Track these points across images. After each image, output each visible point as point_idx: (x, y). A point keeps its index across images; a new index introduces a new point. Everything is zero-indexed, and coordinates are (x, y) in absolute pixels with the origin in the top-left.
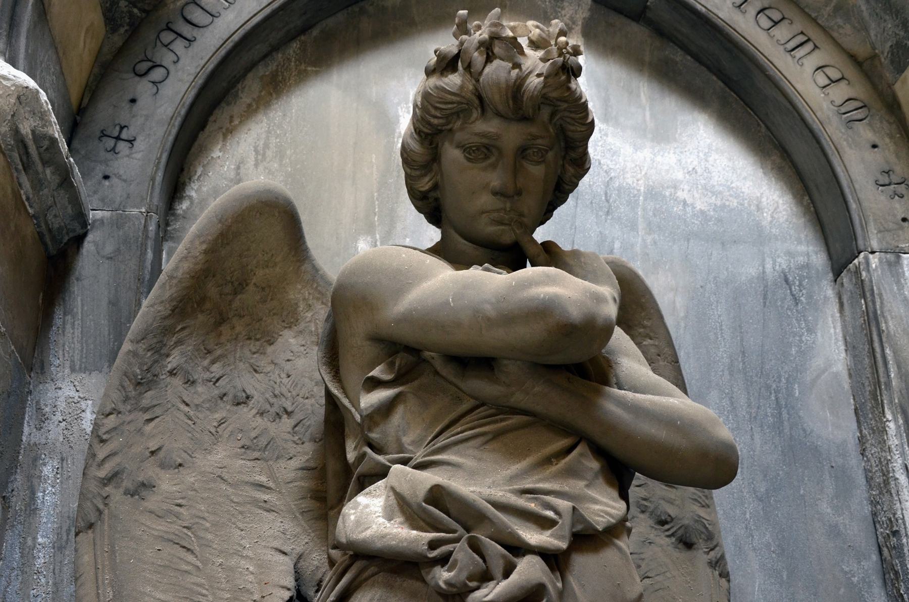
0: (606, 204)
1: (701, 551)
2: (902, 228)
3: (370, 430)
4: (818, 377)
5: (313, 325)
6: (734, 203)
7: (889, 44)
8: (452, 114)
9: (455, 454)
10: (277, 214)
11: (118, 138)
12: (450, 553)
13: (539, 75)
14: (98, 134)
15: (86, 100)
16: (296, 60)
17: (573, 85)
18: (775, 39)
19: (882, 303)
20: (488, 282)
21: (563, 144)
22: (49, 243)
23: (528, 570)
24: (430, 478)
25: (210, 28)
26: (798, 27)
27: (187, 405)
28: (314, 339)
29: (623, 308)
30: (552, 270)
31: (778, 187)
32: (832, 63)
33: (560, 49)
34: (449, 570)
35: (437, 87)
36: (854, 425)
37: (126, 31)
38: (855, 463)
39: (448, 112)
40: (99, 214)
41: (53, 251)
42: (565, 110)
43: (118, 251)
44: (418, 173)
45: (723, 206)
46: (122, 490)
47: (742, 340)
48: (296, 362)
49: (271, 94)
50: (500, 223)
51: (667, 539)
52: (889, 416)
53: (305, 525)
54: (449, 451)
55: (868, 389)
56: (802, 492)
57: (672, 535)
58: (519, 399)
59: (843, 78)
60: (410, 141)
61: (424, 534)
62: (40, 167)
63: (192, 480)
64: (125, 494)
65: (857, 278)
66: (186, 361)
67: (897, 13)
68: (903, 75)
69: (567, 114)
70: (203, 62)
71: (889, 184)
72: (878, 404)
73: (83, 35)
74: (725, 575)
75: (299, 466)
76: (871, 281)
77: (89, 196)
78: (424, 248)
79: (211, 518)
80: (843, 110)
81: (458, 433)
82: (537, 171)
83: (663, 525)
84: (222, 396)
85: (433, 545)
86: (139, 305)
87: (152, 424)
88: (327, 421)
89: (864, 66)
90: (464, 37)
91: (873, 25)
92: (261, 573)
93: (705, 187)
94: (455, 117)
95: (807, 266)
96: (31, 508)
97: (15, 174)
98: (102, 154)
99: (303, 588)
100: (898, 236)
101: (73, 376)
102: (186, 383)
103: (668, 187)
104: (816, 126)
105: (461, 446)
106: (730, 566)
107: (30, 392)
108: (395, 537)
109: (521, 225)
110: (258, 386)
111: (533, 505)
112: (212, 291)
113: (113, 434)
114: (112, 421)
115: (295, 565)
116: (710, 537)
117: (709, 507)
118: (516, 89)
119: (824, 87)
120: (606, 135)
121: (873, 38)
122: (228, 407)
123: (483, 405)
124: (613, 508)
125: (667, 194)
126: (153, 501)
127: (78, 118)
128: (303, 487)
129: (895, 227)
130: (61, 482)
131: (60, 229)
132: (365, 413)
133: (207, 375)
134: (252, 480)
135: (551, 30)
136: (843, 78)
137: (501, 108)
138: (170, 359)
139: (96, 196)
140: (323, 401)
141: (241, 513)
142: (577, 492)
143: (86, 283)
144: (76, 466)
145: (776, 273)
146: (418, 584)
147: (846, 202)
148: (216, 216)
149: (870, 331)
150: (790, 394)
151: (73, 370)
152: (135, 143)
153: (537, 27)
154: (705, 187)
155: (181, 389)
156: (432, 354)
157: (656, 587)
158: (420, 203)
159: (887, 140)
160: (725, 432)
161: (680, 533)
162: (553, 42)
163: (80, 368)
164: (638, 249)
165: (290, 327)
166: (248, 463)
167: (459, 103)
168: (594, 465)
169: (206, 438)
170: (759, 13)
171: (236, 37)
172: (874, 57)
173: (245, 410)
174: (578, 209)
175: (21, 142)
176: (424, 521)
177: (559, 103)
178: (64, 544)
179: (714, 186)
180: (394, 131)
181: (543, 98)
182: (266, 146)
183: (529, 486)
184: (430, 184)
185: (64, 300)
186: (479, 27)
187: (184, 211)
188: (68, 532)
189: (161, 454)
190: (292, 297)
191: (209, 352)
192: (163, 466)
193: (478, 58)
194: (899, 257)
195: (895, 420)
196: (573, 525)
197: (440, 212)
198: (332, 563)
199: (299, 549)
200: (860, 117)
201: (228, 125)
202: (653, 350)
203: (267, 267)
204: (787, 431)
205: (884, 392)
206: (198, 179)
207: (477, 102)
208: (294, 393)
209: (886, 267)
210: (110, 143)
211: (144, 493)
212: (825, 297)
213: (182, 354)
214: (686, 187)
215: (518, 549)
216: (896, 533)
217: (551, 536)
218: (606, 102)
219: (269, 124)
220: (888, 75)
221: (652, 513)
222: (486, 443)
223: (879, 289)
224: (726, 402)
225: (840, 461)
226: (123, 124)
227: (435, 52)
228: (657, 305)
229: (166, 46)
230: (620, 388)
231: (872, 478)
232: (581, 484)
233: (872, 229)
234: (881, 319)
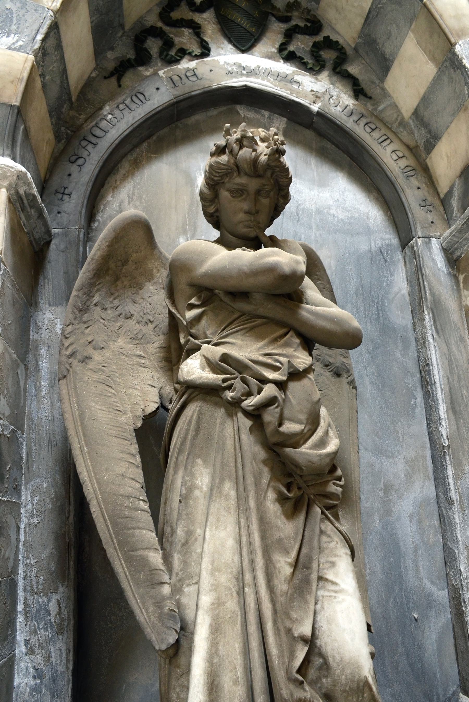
0: (297, 217)
1: (344, 378)
2: (431, 226)
3: (191, 328)
4: (395, 296)
5: (160, 279)
6: (357, 215)
7: (423, 141)
8: (224, 175)
9: (232, 338)
10: (141, 226)
11: (63, 194)
13: (265, 155)
14: (54, 192)
15: (48, 176)
16: (146, 152)
17: (282, 159)
18: (373, 138)
19: (423, 261)
20: (244, 256)
21: (277, 188)
22: (35, 245)
23: (269, 390)
24: (221, 350)
25: (105, 138)
26: (384, 131)
27: (104, 320)
28: (161, 286)
29: (307, 267)
30: (275, 249)
31: (376, 207)
32: (399, 149)
33: (275, 142)
34: (232, 392)
35: (216, 162)
36: (411, 318)
37: (65, 142)
38: (411, 335)
39: (222, 174)
40: (57, 230)
41: (37, 249)
42: (278, 171)
43: (66, 247)
44: (208, 204)
45: (352, 217)
46: (77, 360)
47: (361, 280)
48: (154, 298)
49: (134, 169)
50: (249, 227)
51: (329, 373)
53: (162, 374)
54: (229, 337)
55: (417, 301)
56: (388, 349)
57: (331, 371)
58: (261, 311)
59: (404, 156)
60: (204, 188)
61: (220, 376)
62: (29, 210)
63: (109, 354)
64: (79, 362)
65: (412, 250)
66: (102, 299)
67: (426, 126)
68: (430, 155)
69: (279, 173)
70: (102, 154)
71: (425, 206)
72: (421, 308)
73: (45, 144)
74: (355, 388)
75: (158, 346)
77: (52, 222)
78: (212, 241)
79: (119, 372)
80: (405, 171)
81: (233, 329)
82: (265, 201)
83: (327, 367)
85: (224, 381)
86: (78, 273)
87: (89, 329)
88: (170, 325)
89: (413, 150)
90: (229, 137)
91: (416, 132)
92: (144, 396)
93: (343, 208)
94: (225, 176)
95: (390, 245)
96: (37, 369)
97: (18, 213)
98: (57, 202)
99: (163, 402)
100: (430, 230)
101: (50, 308)
102: (103, 309)
103: (326, 208)
104: (393, 179)
105: (235, 335)
106: (357, 384)
107: (32, 316)
108: (206, 378)
109: (259, 228)
110: (136, 310)
111: (270, 361)
112: (112, 265)
113: (71, 334)
114: (70, 328)
115: (159, 392)
116: (348, 371)
117: (347, 357)
118: (255, 161)
119: (396, 160)
121: (416, 138)
122: (123, 320)
123: (244, 314)
124: (307, 360)
125: (326, 211)
126: (91, 365)
127: (45, 185)
128: (160, 356)
129: (428, 225)
130: (49, 357)
131: (39, 239)
132: (188, 321)
133: (112, 305)
134: (136, 354)
135: (270, 133)
136: (404, 156)
137: (247, 171)
138: (94, 298)
139: (55, 222)
140: (167, 315)
141: (132, 369)
142: (290, 354)
143: (53, 263)
144: (55, 350)
145: (376, 248)
146: (218, 399)
147: (407, 214)
148: (112, 229)
149: (418, 274)
150: (383, 305)
151: (50, 305)
152: (72, 196)
153: (263, 131)
154: (343, 208)
155: (100, 312)
156: (219, 291)
157: (325, 394)
158: (209, 219)
159: (424, 185)
160: (355, 323)
161: (335, 370)
162: (271, 139)
163: (53, 304)
164: (313, 238)
165: (150, 281)
166: (134, 346)
167: (227, 169)
168: (297, 341)
169: (114, 335)
170: (365, 125)
171: (117, 142)
172: (417, 146)
173: (131, 321)
174: (284, 220)
175: (20, 198)
176: (219, 370)
177: (275, 168)
178: (53, 385)
179: (347, 207)
180: (194, 184)
181: (268, 166)
182: (133, 194)
183: (268, 351)
184: (214, 209)
185: (43, 272)
186: (235, 132)
187: (96, 227)
188: (55, 379)
189: (94, 343)
190: (150, 266)
191: (112, 294)
192: (95, 348)
193: (236, 147)
194: (430, 240)
195: (429, 314)
196: (289, 369)
197: (219, 223)
198: (176, 391)
199: (161, 385)
200: (412, 174)
201: (115, 185)
202: (321, 286)
203: (137, 252)
204: (382, 321)
205: (424, 302)
206: (102, 211)
207: (236, 168)
208: (153, 312)
209: (425, 245)
210: (60, 196)
211: (87, 361)
212: (398, 259)
213: (100, 295)
214: (334, 208)
215: (264, 381)
216: (427, 365)
217: (279, 374)
218: (295, 167)
219: (134, 183)
220: (424, 155)
221: (322, 362)
222: (247, 332)
223: (422, 254)
224: (355, 310)
225: (405, 334)
226: (65, 187)
227: (215, 145)
228: (323, 264)
229: (84, 148)
230: (307, 304)
231: (418, 341)
232: (292, 350)
233: (419, 227)
234: (423, 269)
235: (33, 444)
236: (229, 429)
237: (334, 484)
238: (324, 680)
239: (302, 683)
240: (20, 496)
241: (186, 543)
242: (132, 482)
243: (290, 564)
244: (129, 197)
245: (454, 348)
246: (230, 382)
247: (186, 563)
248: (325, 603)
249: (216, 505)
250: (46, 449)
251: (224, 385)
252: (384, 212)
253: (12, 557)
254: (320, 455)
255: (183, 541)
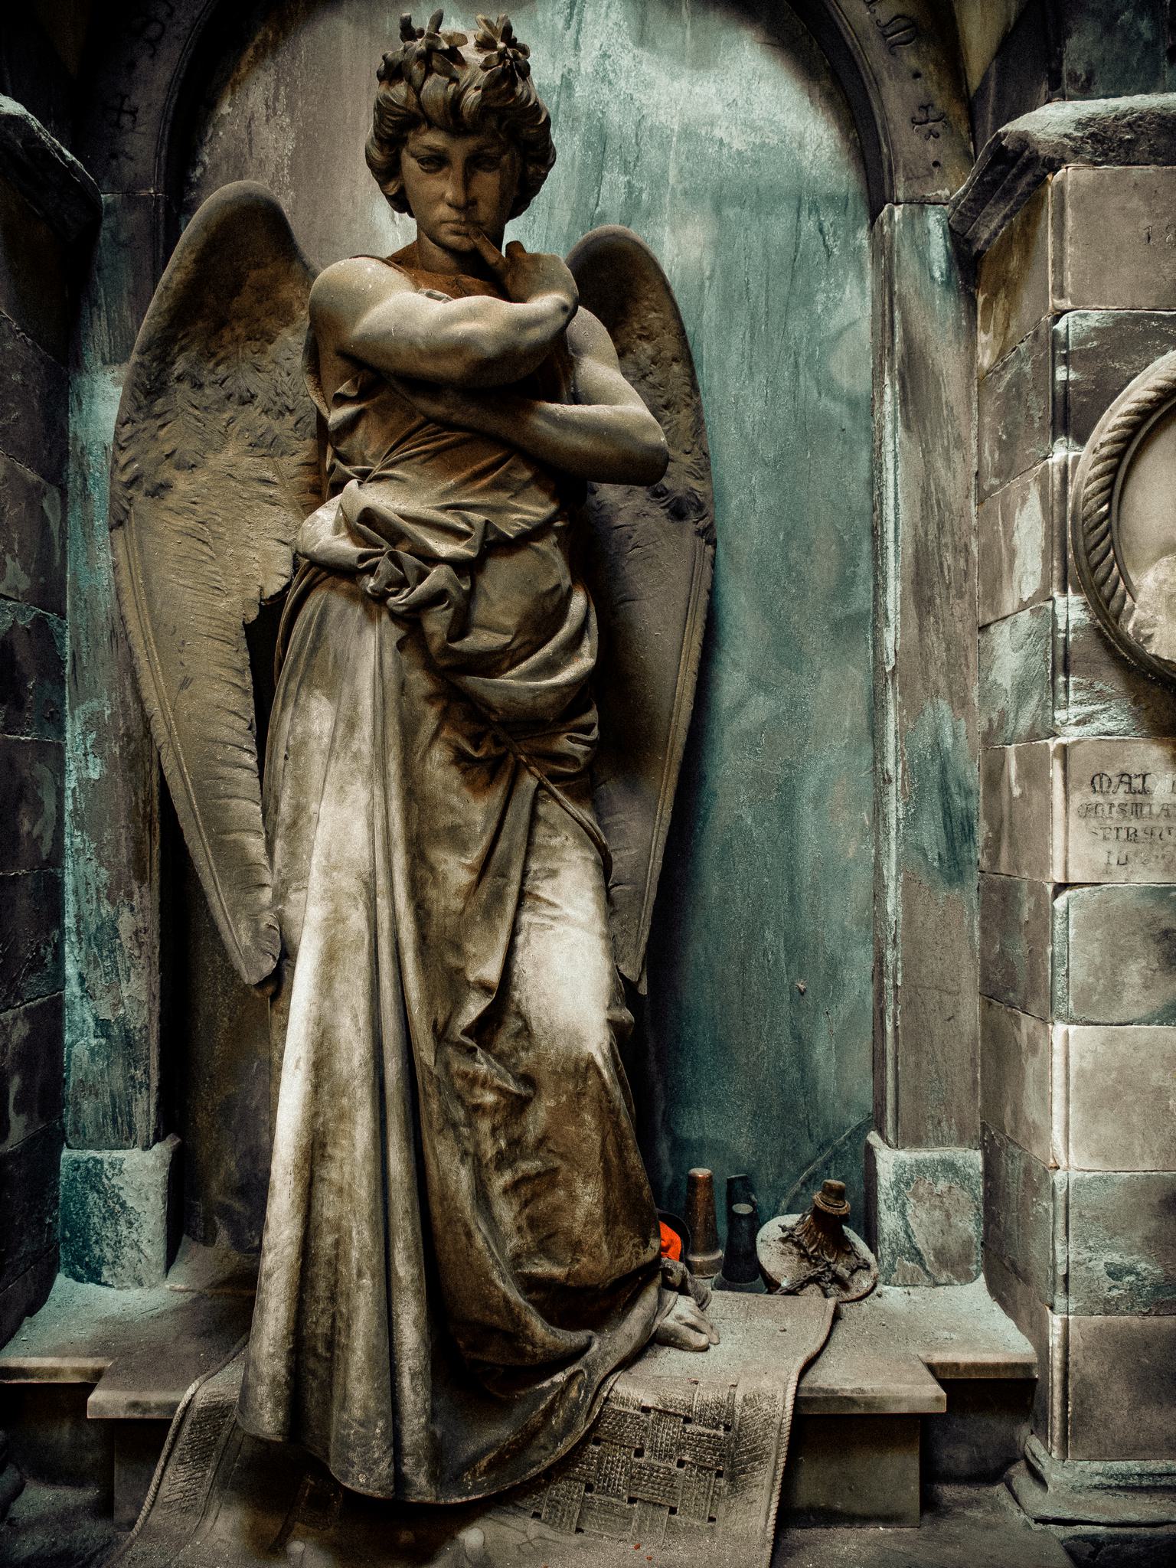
6: (774, 140)
12: (377, 564)
13: (477, 88)
23: (437, 577)
45: (763, 145)
46: (142, 492)
50: (457, 233)
52: (887, 381)
71: (926, 122)
74: (713, 543)
76: (892, 237)
79: (222, 513)
84: (229, 397)
85: (362, 558)
87: (165, 429)
114: (128, 430)
116: (700, 507)
120: (640, 63)
126: (172, 500)
133: (213, 378)
141: (249, 507)
143: (106, 272)
151: (105, 363)
159: (931, 67)
181: (484, 109)
183: (452, 501)
189: (176, 456)
191: (213, 355)
195: (893, 386)
211: (163, 493)
213: (187, 359)
214: (725, 124)
215: (432, 560)
235: (82, 637)
236: (371, 639)
237: (570, 738)
238: (523, 1054)
239: (472, 1050)
240: (61, 731)
241: (294, 823)
242: (232, 718)
243: (471, 868)
244: (268, 107)
245: (940, 463)
246: (373, 560)
247: (293, 855)
248: (533, 934)
249: (338, 767)
250: (107, 646)
251: (362, 566)
252: (841, 129)
253: (48, 837)
254: (555, 688)
255: (288, 821)
